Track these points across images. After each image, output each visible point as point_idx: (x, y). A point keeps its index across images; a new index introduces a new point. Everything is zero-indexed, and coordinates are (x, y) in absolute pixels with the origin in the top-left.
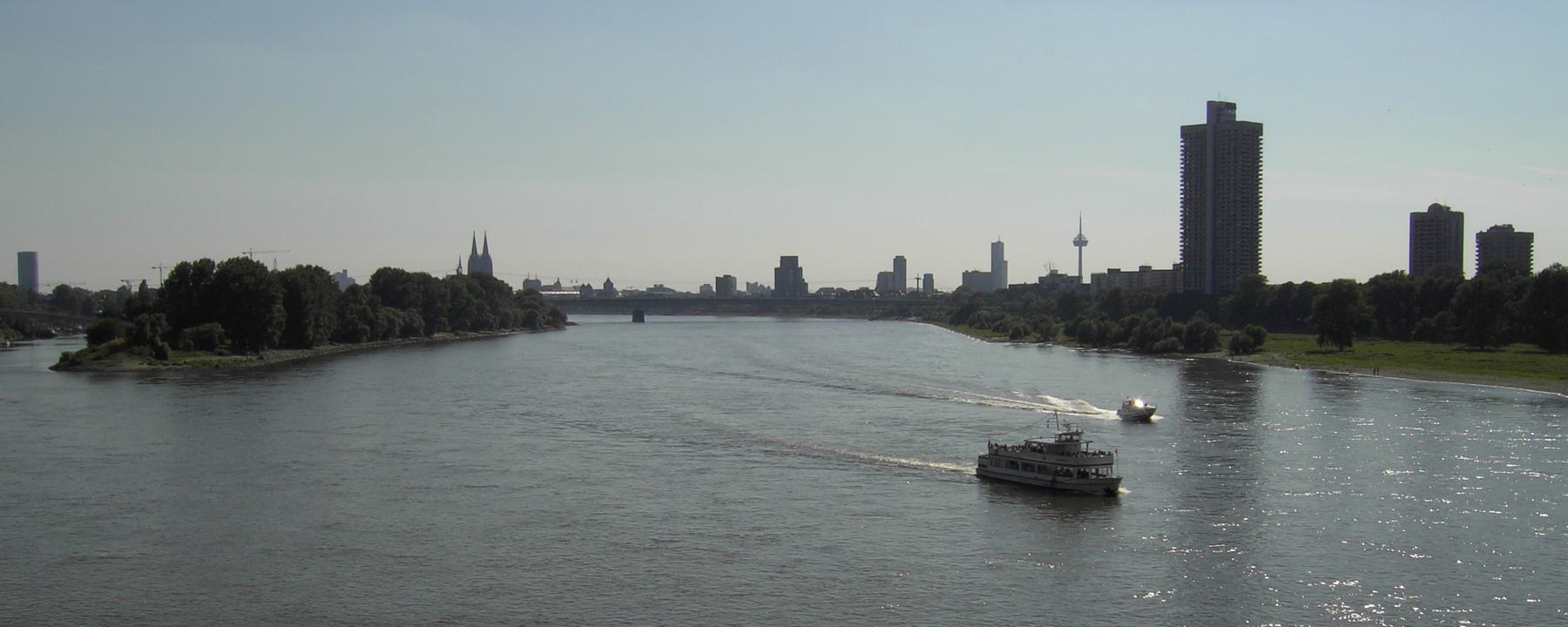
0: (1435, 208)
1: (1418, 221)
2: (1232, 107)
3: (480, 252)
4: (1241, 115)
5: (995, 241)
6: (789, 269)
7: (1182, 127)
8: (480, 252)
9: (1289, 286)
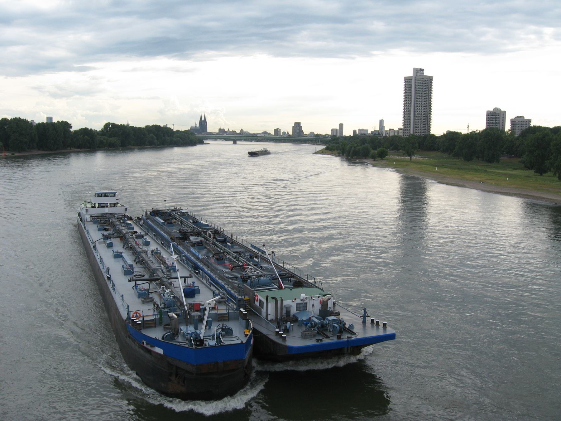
0: (496, 109)
1: (296, 123)
2: (423, 70)
3: (203, 119)
4: (426, 73)
5: (381, 119)
6: (297, 127)
7: (405, 78)
8: (203, 119)
9: (39, 123)
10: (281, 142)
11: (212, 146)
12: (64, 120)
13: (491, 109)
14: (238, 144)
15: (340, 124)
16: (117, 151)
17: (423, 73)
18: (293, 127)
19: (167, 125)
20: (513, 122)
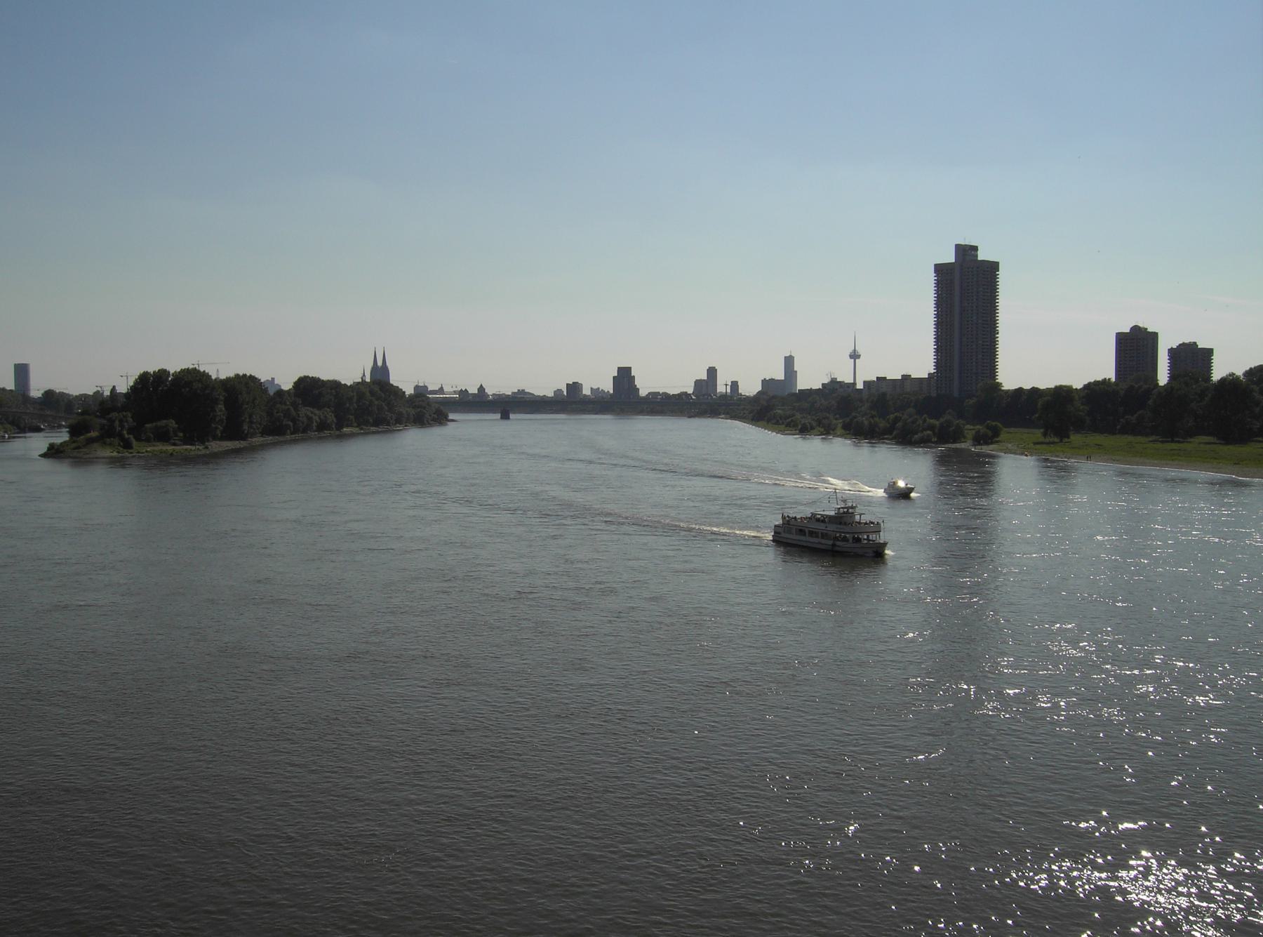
0: (1136, 329)
2: (975, 248)
3: (380, 363)
6: (624, 377)
8: (380, 363)
10: (585, 414)
11: (464, 425)
12: (1058, 384)
13: (1126, 329)
14: (513, 419)
15: (710, 368)
16: (165, 444)
17: (977, 256)
18: (614, 377)
19: (273, 379)
20: (1173, 353)
